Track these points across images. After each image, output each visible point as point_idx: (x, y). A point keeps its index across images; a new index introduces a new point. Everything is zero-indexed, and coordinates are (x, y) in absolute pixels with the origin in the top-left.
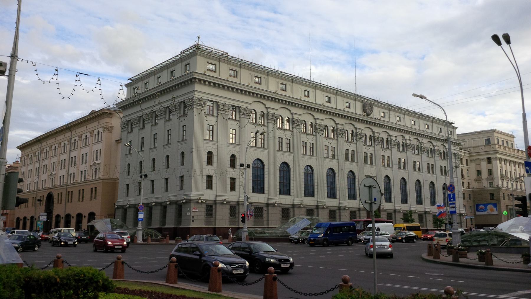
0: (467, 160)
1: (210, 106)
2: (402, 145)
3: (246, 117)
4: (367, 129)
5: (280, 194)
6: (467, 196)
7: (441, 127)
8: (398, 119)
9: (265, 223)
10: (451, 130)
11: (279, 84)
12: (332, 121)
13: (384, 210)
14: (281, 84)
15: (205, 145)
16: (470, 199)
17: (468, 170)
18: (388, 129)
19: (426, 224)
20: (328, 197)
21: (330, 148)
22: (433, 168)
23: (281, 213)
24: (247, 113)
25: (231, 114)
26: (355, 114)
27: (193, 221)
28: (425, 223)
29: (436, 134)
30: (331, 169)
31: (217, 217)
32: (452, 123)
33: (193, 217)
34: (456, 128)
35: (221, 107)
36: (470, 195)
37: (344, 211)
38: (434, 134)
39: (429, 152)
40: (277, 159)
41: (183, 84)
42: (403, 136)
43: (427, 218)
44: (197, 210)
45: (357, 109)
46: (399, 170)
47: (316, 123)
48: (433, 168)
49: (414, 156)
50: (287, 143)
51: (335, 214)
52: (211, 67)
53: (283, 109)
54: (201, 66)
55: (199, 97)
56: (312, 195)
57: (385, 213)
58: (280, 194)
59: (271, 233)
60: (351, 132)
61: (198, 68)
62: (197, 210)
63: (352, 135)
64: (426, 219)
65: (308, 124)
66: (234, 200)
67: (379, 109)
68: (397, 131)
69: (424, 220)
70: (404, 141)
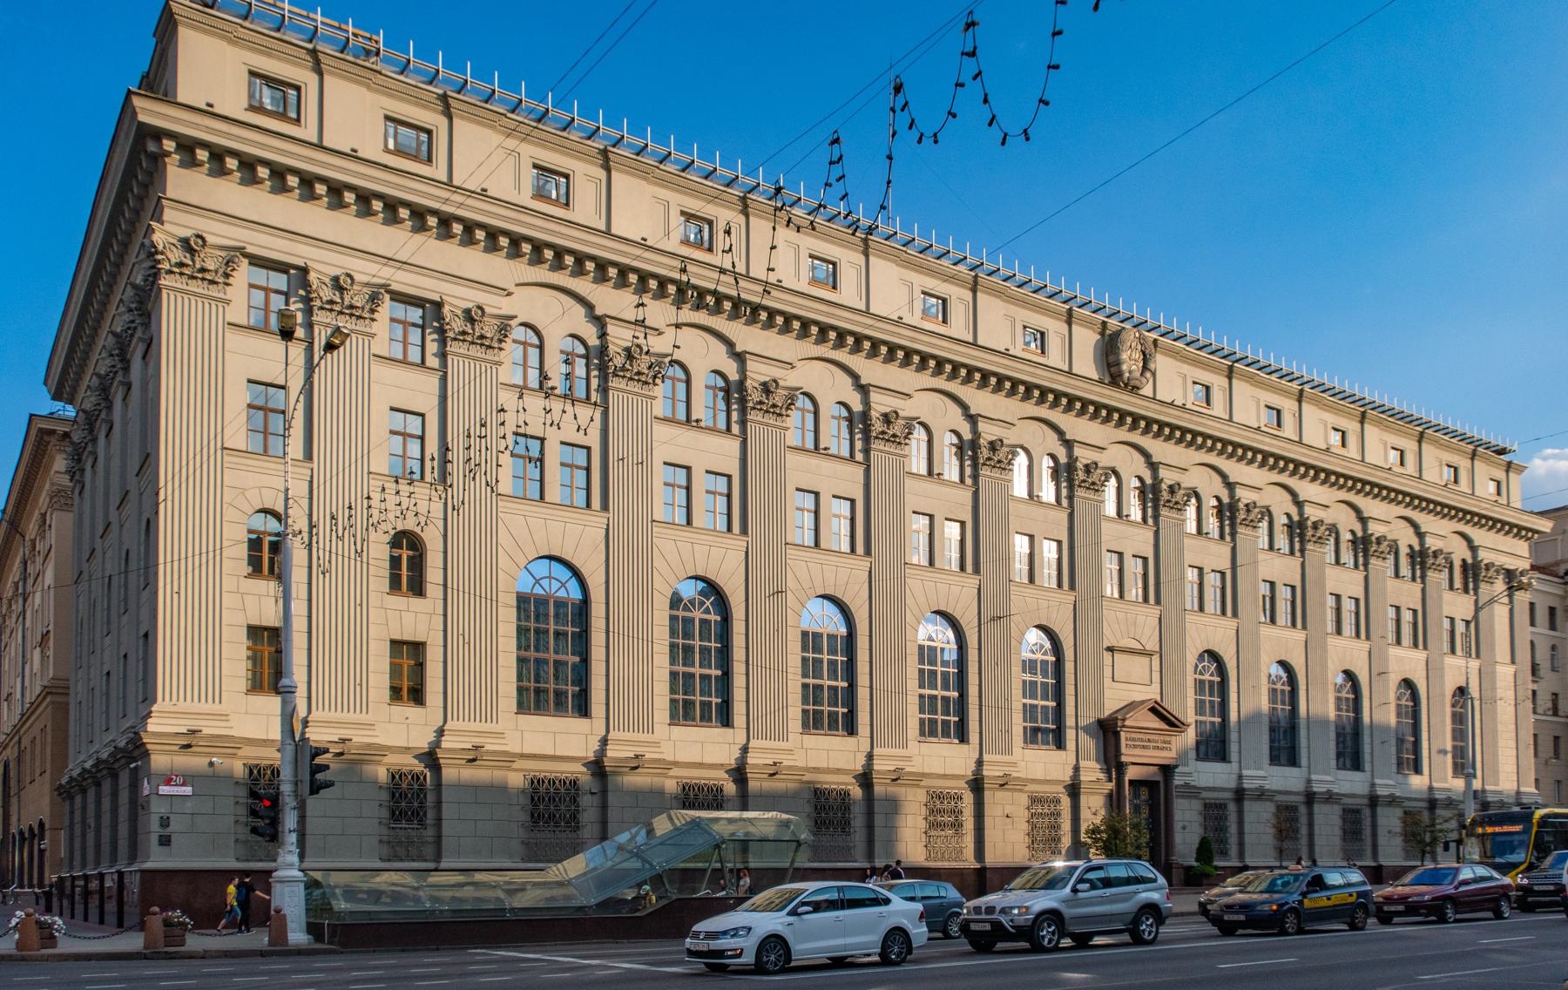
0: (1552, 610)
1: (524, 344)
3: (476, 351)
7: (1455, 459)
9: (1234, 851)
11: (804, 255)
12: (569, 302)
13: (1191, 792)
17: (1553, 648)
20: (1275, 760)
21: (701, 482)
24: (482, 331)
27: (165, 841)
28: (1369, 840)
31: (447, 829)
33: (165, 822)
36: (1556, 738)
37: (1001, 795)
38: (1480, 499)
40: (504, 538)
42: (1415, 526)
43: (1381, 821)
44: (188, 790)
51: (1358, 822)
54: (391, 146)
55: (186, 233)
56: (1293, 762)
57: (1197, 805)
59: (376, 895)
60: (1214, 502)
62: (188, 790)
65: (1404, 551)
67: (1186, 368)
69: (1368, 831)
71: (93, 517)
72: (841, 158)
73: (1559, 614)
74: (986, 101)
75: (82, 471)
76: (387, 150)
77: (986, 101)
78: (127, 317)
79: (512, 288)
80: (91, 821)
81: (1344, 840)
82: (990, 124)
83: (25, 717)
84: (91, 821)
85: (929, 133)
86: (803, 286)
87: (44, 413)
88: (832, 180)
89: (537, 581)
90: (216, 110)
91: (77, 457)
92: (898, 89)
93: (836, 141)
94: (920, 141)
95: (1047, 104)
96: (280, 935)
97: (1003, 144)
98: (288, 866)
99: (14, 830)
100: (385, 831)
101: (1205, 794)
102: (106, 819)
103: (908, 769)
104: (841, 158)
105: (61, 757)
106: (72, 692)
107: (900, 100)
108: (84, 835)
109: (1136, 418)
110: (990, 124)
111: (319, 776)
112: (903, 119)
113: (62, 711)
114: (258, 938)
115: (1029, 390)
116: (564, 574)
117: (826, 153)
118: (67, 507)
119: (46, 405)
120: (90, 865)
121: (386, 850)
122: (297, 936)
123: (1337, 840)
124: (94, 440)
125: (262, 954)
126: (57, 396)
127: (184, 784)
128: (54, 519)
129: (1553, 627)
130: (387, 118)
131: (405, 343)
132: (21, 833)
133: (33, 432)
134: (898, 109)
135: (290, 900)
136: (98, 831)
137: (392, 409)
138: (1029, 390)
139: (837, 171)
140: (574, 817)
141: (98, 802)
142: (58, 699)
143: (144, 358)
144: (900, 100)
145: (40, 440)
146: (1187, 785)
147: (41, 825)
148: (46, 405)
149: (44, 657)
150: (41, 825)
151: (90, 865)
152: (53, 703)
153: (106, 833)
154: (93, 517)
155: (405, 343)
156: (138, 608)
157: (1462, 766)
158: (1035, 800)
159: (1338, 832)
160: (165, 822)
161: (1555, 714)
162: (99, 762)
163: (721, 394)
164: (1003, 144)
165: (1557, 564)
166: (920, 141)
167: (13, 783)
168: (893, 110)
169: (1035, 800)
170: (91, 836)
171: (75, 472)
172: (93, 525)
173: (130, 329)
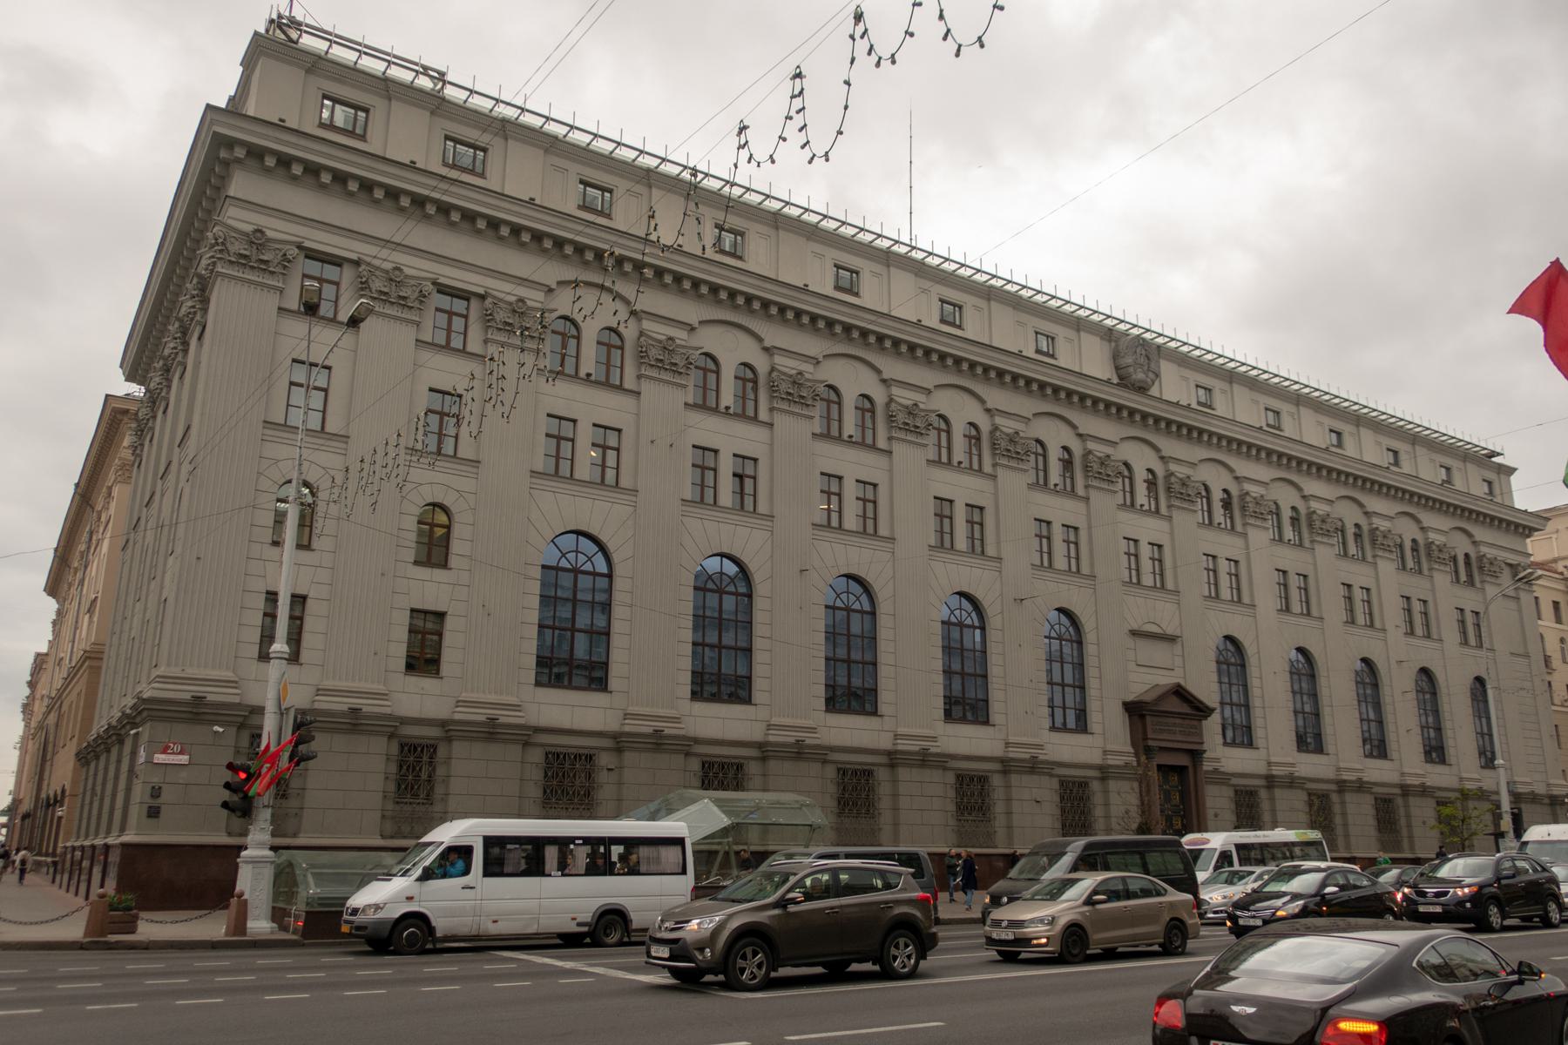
0: (1556, 604)
1: (563, 335)
2: (1413, 550)
4: (1405, 521)
5: (696, 695)
10: (1491, 476)
11: (574, 179)
12: (966, 397)
13: (1221, 778)
14: (838, 267)
17: (1562, 640)
18: (1469, 518)
19: (1411, 837)
25: (1506, 578)
29: (1477, 498)
30: (1228, 638)
32: (1494, 454)
33: (156, 793)
34: (1511, 471)
35: (1096, 467)
39: (1408, 553)
44: (184, 759)
45: (1094, 363)
46: (1351, 629)
47: (995, 428)
49: (1345, 565)
52: (341, 116)
53: (842, 362)
56: (1319, 749)
58: (696, 695)
61: (1516, 495)
62: (184, 759)
64: (1408, 816)
66: (607, 728)
68: (1329, 479)
70: (1419, 537)
72: (801, 92)
73: (1562, 606)
74: (941, 17)
76: (445, 164)
77: (941, 17)
78: (190, 303)
79: (554, 286)
80: (98, 789)
81: (1379, 831)
82: (945, 38)
83: (68, 680)
84: (98, 789)
86: (829, 290)
87: (120, 394)
88: (793, 113)
89: (564, 555)
90: (287, 124)
91: (140, 432)
92: (858, 17)
93: (799, 75)
94: (878, 65)
95: (1002, 8)
96: (239, 925)
97: (957, 55)
98: (257, 845)
99: (43, 795)
100: (390, 806)
101: (1234, 781)
103: (933, 750)
104: (801, 92)
105: (88, 720)
106: (105, 656)
107: (860, 29)
109: (1145, 416)
110: (945, 38)
112: (862, 46)
113: (96, 672)
114: (213, 927)
116: (590, 547)
117: (787, 88)
119: (125, 388)
120: (115, 833)
121: (389, 827)
122: (260, 925)
124: (154, 417)
125: (214, 945)
127: (181, 753)
128: (115, 491)
129: (1559, 620)
130: (447, 138)
131: (449, 330)
133: (108, 412)
134: (857, 36)
135: (253, 882)
136: (102, 799)
137: (431, 390)
139: (797, 103)
142: (95, 663)
143: (199, 338)
144: (860, 29)
145: (114, 416)
146: (1216, 771)
147: (63, 791)
148: (125, 388)
150: (63, 791)
151: (115, 833)
152: (90, 667)
153: (107, 801)
155: (449, 330)
156: (164, 572)
157: (1488, 759)
159: (1372, 821)
160: (156, 793)
164: (957, 55)
165: (1555, 561)
166: (878, 65)
167: (50, 748)
168: (852, 37)
169: (1064, 783)
170: (96, 805)
171: (136, 449)
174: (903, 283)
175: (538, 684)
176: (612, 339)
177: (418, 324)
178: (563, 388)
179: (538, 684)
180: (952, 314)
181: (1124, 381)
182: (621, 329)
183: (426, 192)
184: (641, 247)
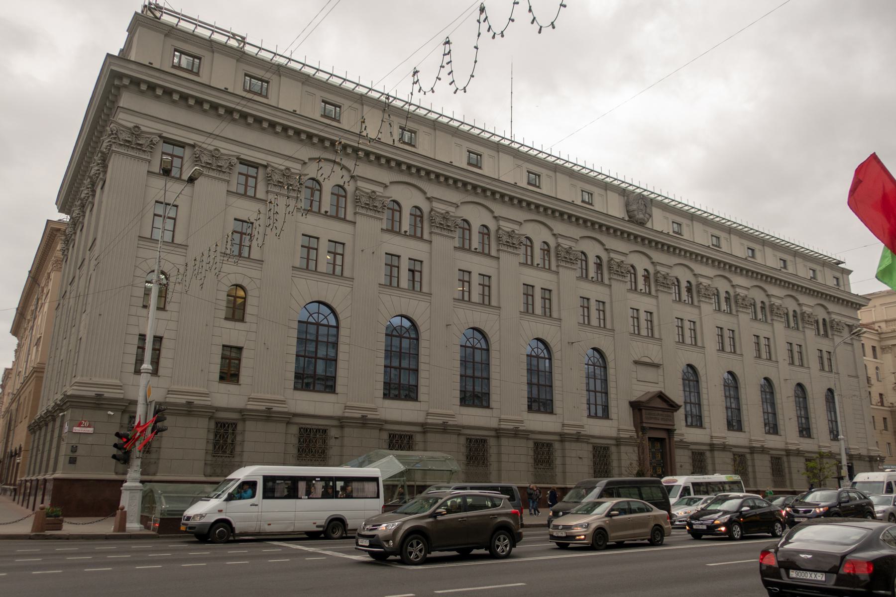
0: (874, 348)
6: (880, 425)
8: (750, 254)
10: (838, 275)
12: (542, 227)
13: (684, 445)
15: (226, 268)
16: (886, 428)
17: (877, 368)
21: (593, 304)
22: (822, 364)
23: (591, 456)
25: (846, 333)
26: (498, 180)
27: (73, 461)
30: (689, 366)
32: (840, 262)
34: (849, 272)
36: (885, 419)
41: (769, 279)
44: (91, 430)
45: (615, 208)
47: (558, 245)
48: (822, 364)
50: (647, 320)
56: (740, 429)
58: (386, 396)
62: (91, 430)
63: (689, 290)
64: (789, 467)
66: (335, 414)
68: (747, 276)
70: (766, 300)
71: (69, 273)
72: (449, 52)
74: (530, 10)
75: (68, 249)
76: (245, 90)
77: (530, 10)
78: (96, 168)
79: (307, 161)
80: (41, 447)
81: (773, 475)
82: (532, 23)
83: (24, 384)
85: (498, 32)
86: (464, 165)
88: (444, 64)
92: (482, 10)
93: (448, 42)
94: (494, 37)
95: (565, 6)
96: (122, 526)
97: (540, 32)
98: (133, 480)
99: (9, 450)
100: (210, 458)
102: (47, 448)
104: (449, 52)
105: (35, 407)
107: (483, 16)
108: (36, 455)
109: (643, 239)
111: (159, 424)
112: (484, 26)
113: (40, 380)
114: (107, 527)
115: (585, 222)
116: (326, 311)
117: (441, 49)
118: (59, 270)
119: (58, 216)
122: (133, 526)
123: (769, 476)
124: (75, 233)
125: (107, 537)
126: (61, 210)
127: (89, 427)
128: (52, 276)
130: (246, 75)
131: (246, 185)
132: (11, 452)
133: (48, 230)
134: (482, 21)
135: (130, 500)
136: (43, 453)
137: (235, 219)
138: (585, 222)
140: (323, 452)
141: (45, 435)
144: (483, 16)
145: (52, 232)
146: (681, 441)
147: (20, 448)
148: (58, 216)
149: (37, 350)
150: (20, 448)
152: (36, 377)
153: (46, 454)
154: (69, 273)
155: (246, 185)
158: (596, 448)
159: (769, 470)
160: (74, 449)
161: (882, 405)
162: (48, 411)
163: (419, 219)
164: (540, 32)
166: (494, 37)
168: (479, 21)
169: (596, 448)
171: (65, 251)
172: (68, 277)
173: (97, 175)
174: (506, 161)
175: (295, 388)
176: (340, 192)
177: (228, 182)
178: (311, 219)
179: (295, 388)
180: (534, 179)
181: (632, 219)
182: (346, 186)
183: (233, 106)
184: (357, 139)
